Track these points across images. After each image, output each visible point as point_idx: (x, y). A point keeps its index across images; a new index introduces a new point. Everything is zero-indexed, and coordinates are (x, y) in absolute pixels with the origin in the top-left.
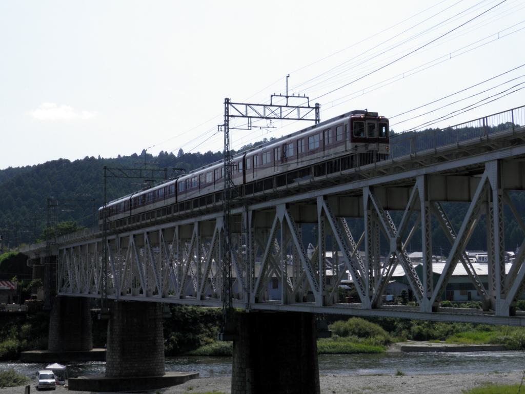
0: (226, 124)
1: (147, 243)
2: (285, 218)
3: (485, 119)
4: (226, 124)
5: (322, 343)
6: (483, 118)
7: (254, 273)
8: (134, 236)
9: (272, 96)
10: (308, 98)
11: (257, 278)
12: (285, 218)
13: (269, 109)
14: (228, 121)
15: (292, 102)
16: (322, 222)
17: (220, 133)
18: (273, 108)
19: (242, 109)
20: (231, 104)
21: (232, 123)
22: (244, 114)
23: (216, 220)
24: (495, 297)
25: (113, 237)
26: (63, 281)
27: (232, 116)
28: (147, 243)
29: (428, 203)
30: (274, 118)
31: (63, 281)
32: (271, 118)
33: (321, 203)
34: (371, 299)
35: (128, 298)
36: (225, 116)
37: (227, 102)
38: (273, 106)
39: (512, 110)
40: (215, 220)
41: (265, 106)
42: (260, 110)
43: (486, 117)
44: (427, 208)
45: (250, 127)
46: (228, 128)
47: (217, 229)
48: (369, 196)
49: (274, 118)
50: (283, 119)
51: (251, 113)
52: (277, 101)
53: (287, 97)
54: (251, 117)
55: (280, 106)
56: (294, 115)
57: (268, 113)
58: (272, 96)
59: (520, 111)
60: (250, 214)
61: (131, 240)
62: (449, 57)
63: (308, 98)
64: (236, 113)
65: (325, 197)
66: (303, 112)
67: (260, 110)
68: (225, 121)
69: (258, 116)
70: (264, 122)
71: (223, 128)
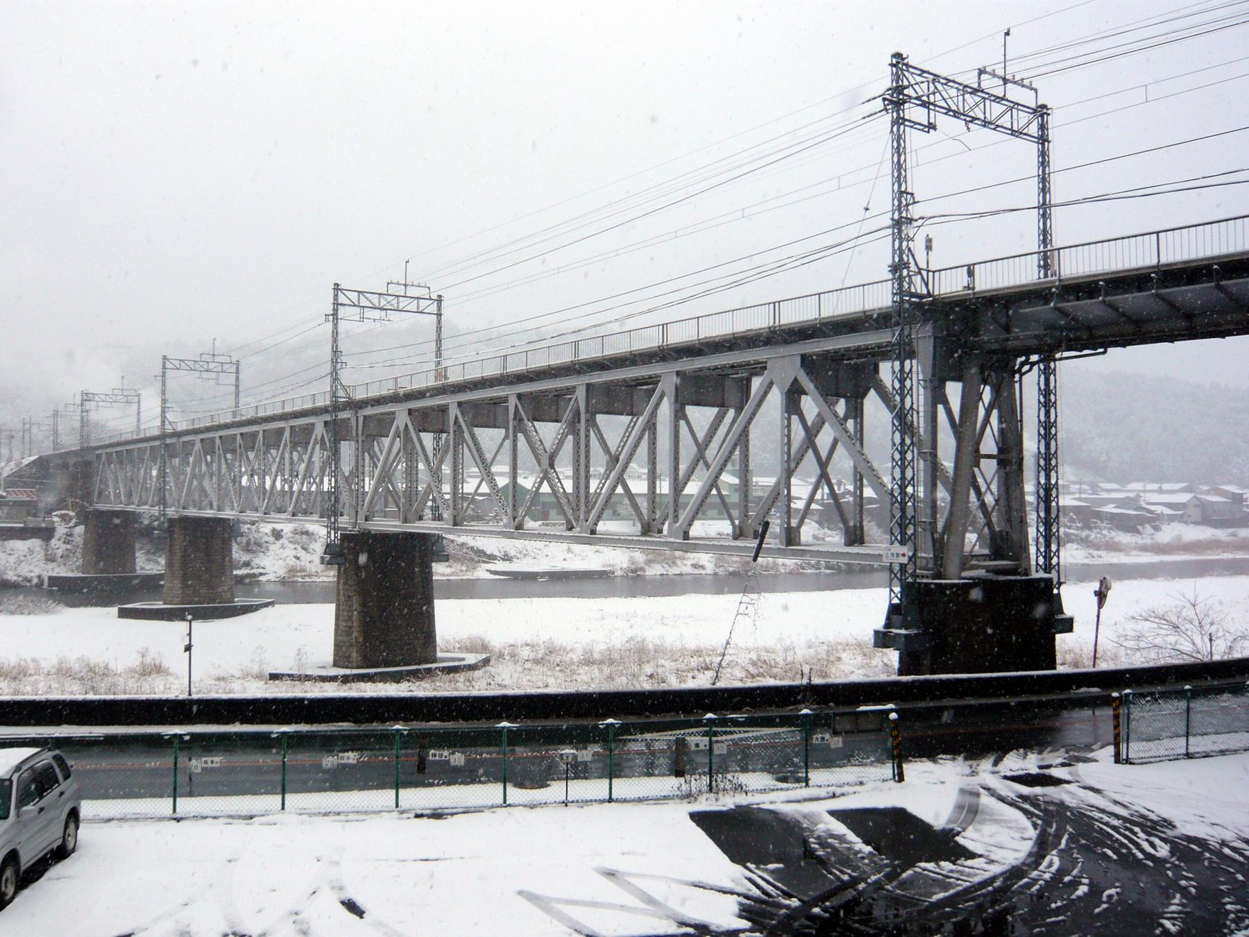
0: (335, 314)
1: (219, 449)
2: (406, 425)
3: (777, 304)
4: (335, 314)
5: (440, 570)
6: (663, 325)
7: (363, 487)
8: (202, 440)
9: (388, 283)
10: (429, 288)
11: (367, 492)
12: (406, 425)
13: (386, 300)
14: (337, 310)
15: (412, 292)
16: (455, 432)
17: (327, 323)
18: (390, 298)
19: (354, 296)
20: (341, 290)
21: (342, 312)
22: (356, 303)
23: (660, 376)
24: (298, 558)
25: (174, 440)
26: (100, 494)
27: (342, 305)
28: (219, 449)
29: (588, 415)
30: (391, 310)
31: (100, 494)
32: (386, 309)
33: (454, 411)
34: (514, 520)
35: (192, 512)
36: (334, 304)
37: (337, 287)
38: (390, 295)
39: (819, 294)
40: (313, 424)
41: (380, 294)
42: (375, 299)
43: (779, 302)
44: (588, 421)
45: (362, 319)
46: (337, 319)
47: (316, 436)
48: (516, 405)
49: (391, 310)
50: (401, 311)
51: (364, 302)
52: (394, 289)
53: (406, 285)
54: (364, 307)
55: (397, 296)
56: (413, 307)
57: (383, 303)
58: (388, 283)
59: (857, 292)
60: (361, 420)
61: (198, 446)
62: (615, 253)
63: (429, 288)
64: (346, 301)
65: (460, 404)
66: (423, 303)
67: (375, 299)
68: (334, 309)
69: (372, 306)
70: (377, 314)
71: (331, 318)
